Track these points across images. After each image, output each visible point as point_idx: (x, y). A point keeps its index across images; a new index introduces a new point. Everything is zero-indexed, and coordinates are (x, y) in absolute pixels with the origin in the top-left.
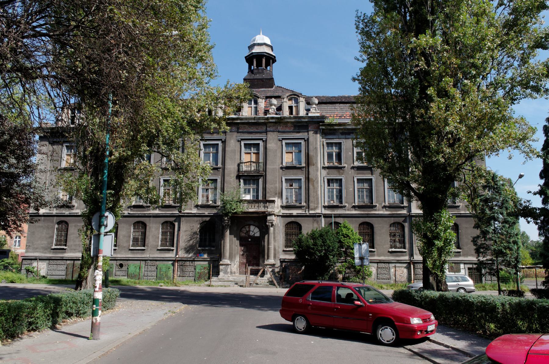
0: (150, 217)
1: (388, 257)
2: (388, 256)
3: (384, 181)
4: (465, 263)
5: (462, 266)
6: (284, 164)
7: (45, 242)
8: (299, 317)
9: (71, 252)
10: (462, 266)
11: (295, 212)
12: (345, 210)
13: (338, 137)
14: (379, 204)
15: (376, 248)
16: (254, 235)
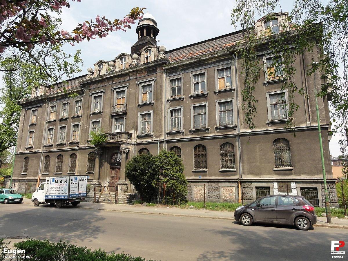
0: (64, 151)
1: (219, 176)
2: (219, 176)
4: (296, 182)
5: (293, 185)
6: (140, 103)
7: (19, 170)
10: (293, 185)
11: (144, 141)
12: (183, 135)
14: (211, 127)
15: (208, 168)
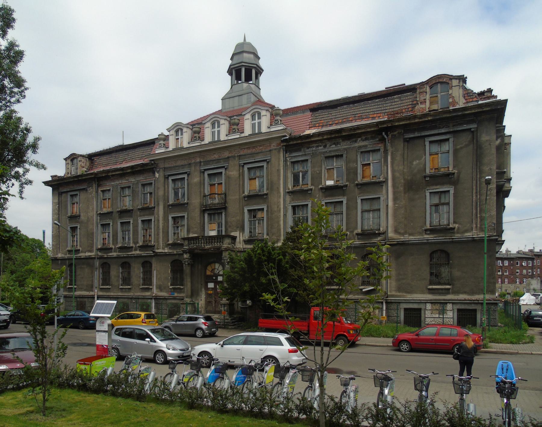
3: (204, 217)
8: (161, 354)
9: (79, 291)
13: (304, 153)
16: (219, 272)
